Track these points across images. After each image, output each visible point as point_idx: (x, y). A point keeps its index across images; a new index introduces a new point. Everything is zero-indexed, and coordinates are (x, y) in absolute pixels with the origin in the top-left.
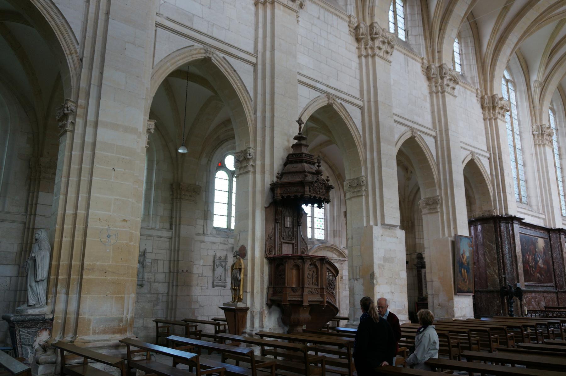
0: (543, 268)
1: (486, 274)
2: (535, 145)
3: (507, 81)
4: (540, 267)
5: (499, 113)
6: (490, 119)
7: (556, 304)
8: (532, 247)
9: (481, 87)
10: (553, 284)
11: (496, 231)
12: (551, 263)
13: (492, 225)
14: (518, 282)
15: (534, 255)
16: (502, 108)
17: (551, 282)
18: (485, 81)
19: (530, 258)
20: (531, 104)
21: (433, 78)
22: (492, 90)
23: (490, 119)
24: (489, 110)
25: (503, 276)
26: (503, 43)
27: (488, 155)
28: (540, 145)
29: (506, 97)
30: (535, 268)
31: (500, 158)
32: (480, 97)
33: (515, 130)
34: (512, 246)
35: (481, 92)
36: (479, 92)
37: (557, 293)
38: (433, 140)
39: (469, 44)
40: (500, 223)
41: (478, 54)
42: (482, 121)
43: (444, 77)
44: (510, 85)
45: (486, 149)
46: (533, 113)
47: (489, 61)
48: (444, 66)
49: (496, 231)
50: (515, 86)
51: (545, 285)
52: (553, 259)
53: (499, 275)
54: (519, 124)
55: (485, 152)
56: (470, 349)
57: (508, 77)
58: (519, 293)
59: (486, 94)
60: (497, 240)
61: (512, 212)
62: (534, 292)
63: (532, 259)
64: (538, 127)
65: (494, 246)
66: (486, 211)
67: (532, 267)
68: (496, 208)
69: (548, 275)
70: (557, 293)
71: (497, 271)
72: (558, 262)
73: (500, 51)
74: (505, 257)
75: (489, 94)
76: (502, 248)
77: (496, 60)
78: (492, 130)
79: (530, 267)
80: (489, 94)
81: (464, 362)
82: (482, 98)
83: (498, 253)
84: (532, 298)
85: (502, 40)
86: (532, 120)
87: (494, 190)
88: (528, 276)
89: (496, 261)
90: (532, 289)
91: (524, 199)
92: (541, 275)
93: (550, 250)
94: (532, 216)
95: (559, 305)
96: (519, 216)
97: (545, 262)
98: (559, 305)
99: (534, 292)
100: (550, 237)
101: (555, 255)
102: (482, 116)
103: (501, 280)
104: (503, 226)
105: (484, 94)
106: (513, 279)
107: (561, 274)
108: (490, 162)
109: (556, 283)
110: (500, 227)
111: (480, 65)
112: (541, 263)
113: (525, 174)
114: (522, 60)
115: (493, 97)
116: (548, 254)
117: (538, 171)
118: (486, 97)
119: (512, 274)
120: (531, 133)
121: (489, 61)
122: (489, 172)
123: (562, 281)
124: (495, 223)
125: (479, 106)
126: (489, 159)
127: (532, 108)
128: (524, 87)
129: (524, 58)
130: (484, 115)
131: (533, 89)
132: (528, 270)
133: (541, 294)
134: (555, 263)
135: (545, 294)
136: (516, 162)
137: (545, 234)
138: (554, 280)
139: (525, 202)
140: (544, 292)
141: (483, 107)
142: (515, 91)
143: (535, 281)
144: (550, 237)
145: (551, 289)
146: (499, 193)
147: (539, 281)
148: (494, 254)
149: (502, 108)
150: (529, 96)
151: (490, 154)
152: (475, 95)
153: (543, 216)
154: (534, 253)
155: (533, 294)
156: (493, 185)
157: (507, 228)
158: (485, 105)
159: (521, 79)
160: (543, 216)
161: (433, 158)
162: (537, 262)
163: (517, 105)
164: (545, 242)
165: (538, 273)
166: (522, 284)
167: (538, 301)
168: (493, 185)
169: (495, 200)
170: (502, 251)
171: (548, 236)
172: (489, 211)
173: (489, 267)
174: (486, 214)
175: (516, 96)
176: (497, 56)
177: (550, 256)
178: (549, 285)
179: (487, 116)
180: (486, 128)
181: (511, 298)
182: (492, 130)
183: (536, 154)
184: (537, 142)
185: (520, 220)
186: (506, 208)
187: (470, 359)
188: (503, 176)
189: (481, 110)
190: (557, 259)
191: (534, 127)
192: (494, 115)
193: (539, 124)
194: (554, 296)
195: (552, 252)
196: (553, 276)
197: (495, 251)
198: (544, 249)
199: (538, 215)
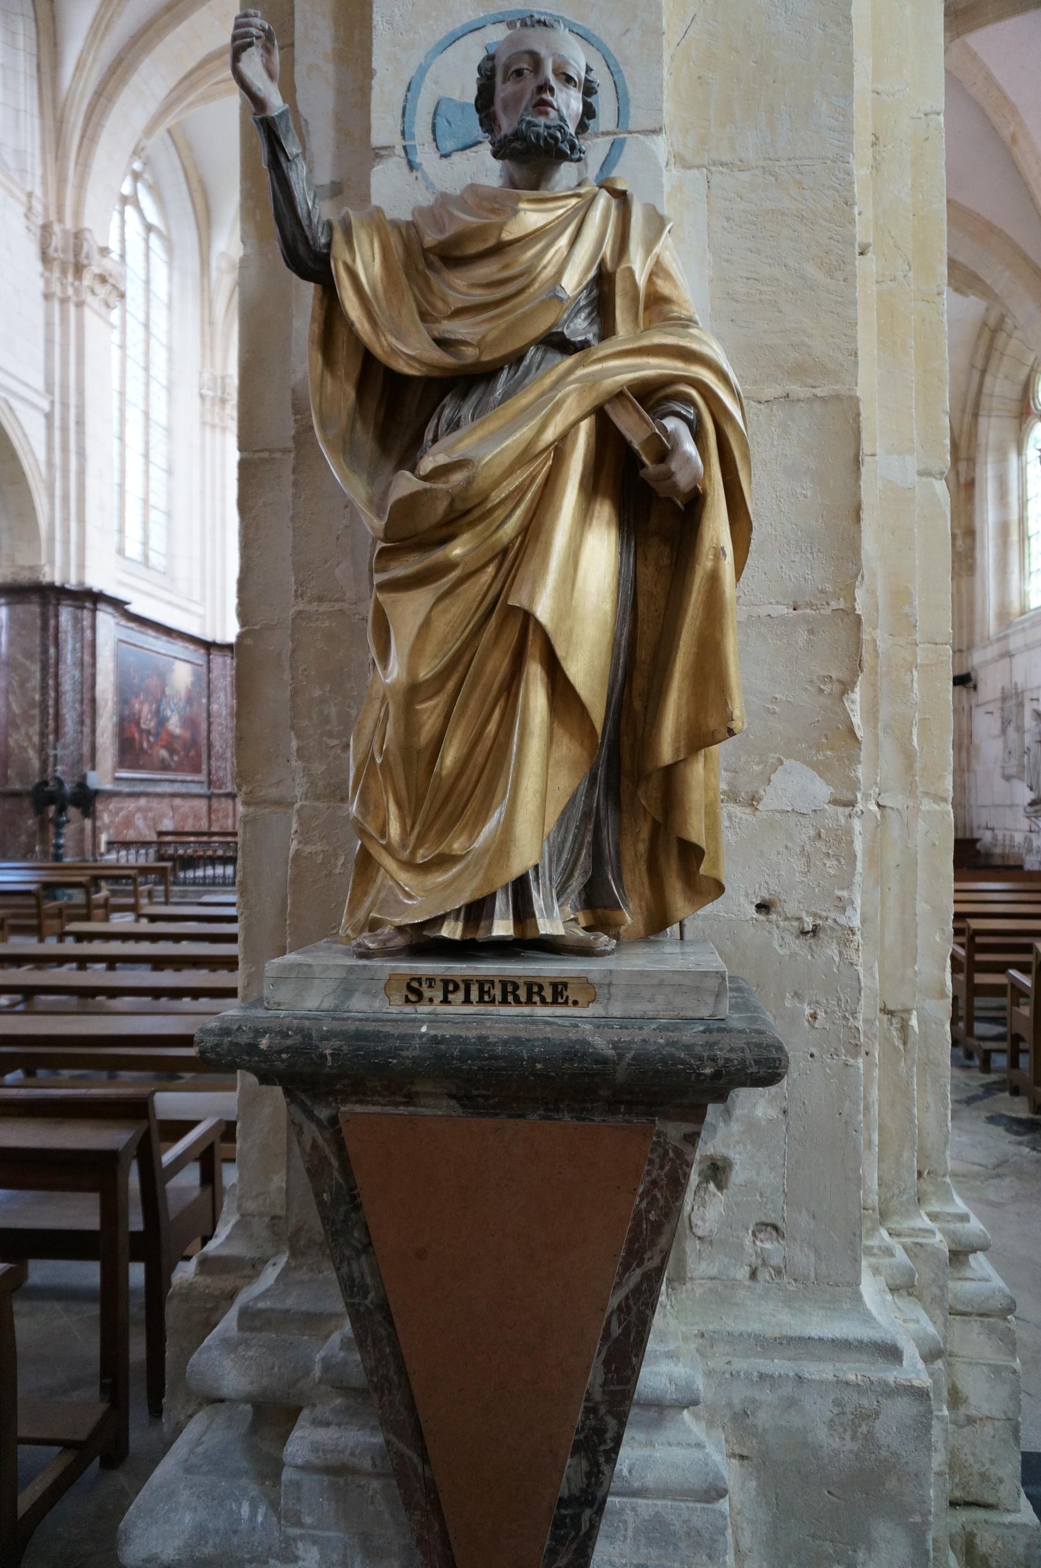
0: (178, 737)
1: (7, 746)
2: (204, 424)
3: (149, 228)
4: (172, 736)
5: (93, 292)
6: (64, 301)
7: (204, 825)
8: (153, 682)
9: (46, 193)
10: (202, 777)
11: (45, 627)
12: (204, 726)
13: (36, 609)
14: (93, 768)
15: (159, 702)
16: (103, 279)
17: (197, 770)
18: (61, 180)
19: (146, 709)
20: (207, 312)
21: (55, 259)
22: (78, 214)
23: (64, 301)
24: (64, 273)
25: (51, 752)
26: (123, 81)
27: (45, 405)
28: (213, 426)
29: (114, 245)
30: (157, 735)
31: (80, 423)
32: (40, 221)
33: (153, 371)
34: (88, 671)
35: (46, 208)
36: (38, 207)
37: (209, 797)
38: (42, 420)
39: (21, 40)
40: (58, 604)
41: (48, 93)
42: (40, 299)
43: (84, 267)
44: (154, 241)
45: (39, 384)
46: (208, 339)
47: (76, 120)
48: (87, 235)
49: (45, 627)
50: (170, 248)
51: (180, 778)
52: (209, 715)
53: (42, 749)
54: (170, 360)
55: (36, 391)
56: (87, 918)
57: (153, 216)
58: (86, 800)
59: (61, 220)
60: (45, 651)
61: (96, 581)
62: (147, 795)
63: (150, 711)
64: (214, 379)
65: (36, 668)
66: (23, 568)
67: (149, 733)
68: (51, 562)
69: (192, 753)
70: (209, 797)
71: (36, 739)
72: (220, 724)
73: (111, 100)
74: (62, 701)
75: (69, 224)
76: (56, 676)
77: (99, 125)
78: (65, 334)
79: (141, 731)
80: (69, 224)
81: (70, 947)
82: (46, 229)
83: (44, 689)
84: (139, 809)
85: (119, 69)
86: (203, 356)
87: (52, 509)
88: (130, 751)
89: (36, 712)
90: (139, 788)
91: (154, 559)
92: (172, 751)
93: (205, 693)
94: (169, 603)
95: (210, 826)
96: (111, 591)
97: (189, 723)
98: (210, 826)
99: (147, 795)
100: (209, 662)
101: (215, 707)
102: (40, 284)
103: (44, 763)
104: (66, 615)
105: (53, 216)
106: (80, 760)
107: (224, 753)
108: (50, 427)
109: (209, 773)
110: (57, 616)
111: (50, 123)
112: (174, 725)
113: (170, 494)
114: (195, 185)
115: (78, 236)
116: (200, 704)
117: (203, 493)
118: (57, 228)
119: (80, 745)
120: (196, 390)
121: (76, 120)
122: (41, 454)
123: (225, 769)
124: (44, 604)
125: (32, 249)
126: (49, 416)
127: (207, 326)
128: (193, 263)
129: (201, 182)
130: (47, 282)
131: (214, 274)
132: (133, 738)
133: (167, 801)
134: (214, 727)
135: (177, 802)
136: (146, 456)
137: (198, 655)
138: (204, 767)
139: (161, 568)
140: (174, 795)
141: (45, 258)
142: (170, 263)
143: (153, 769)
144: (209, 662)
145: (196, 789)
146: (66, 520)
147: (164, 767)
148: (34, 689)
149: (103, 279)
150: (203, 291)
151: (52, 403)
152: (21, 210)
153: (200, 610)
154: (159, 697)
155: (143, 801)
156: (51, 496)
157: (77, 621)
158: (51, 251)
159: (188, 237)
160: (200, 610)
161: (38, 466)
162: (162, 721)
163: (169, 306)
164: (197, 676)
165: (163, 747)
166: (100, 779)
167: (154, 819)
168: (51, 496)
169: (51, 539)
170: (57, 685)
171: (205, 658)
172: (32, 568)
173: (17, 727)
174: (24, 577)
175: (170, 279)
176: (104, 114)
177: (204, 708)
178: (189, 778)
179: (56, 288)
180: (49, 325)
181: (61, 810)
182: (65, 334)
183: (203, 448)
184: (208, 418)
185: (118, 605)
186: (81, 567)
187: (81, 937)
188: (82, 473)
189: (38, 266)
190: (221, 716)
191: (206, 376)
192: (77, 291)
193: (218, 372)
194: (202, 804)
195: (209, 697)
196: (204, 757)
197: (36, 681)
198: (189, 692)
199: (184, 603)
